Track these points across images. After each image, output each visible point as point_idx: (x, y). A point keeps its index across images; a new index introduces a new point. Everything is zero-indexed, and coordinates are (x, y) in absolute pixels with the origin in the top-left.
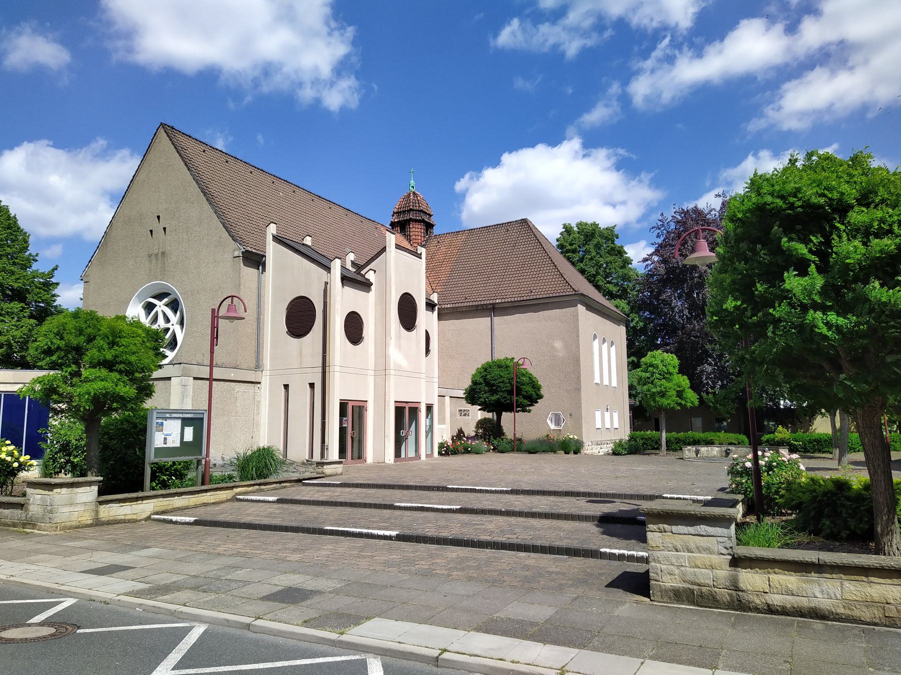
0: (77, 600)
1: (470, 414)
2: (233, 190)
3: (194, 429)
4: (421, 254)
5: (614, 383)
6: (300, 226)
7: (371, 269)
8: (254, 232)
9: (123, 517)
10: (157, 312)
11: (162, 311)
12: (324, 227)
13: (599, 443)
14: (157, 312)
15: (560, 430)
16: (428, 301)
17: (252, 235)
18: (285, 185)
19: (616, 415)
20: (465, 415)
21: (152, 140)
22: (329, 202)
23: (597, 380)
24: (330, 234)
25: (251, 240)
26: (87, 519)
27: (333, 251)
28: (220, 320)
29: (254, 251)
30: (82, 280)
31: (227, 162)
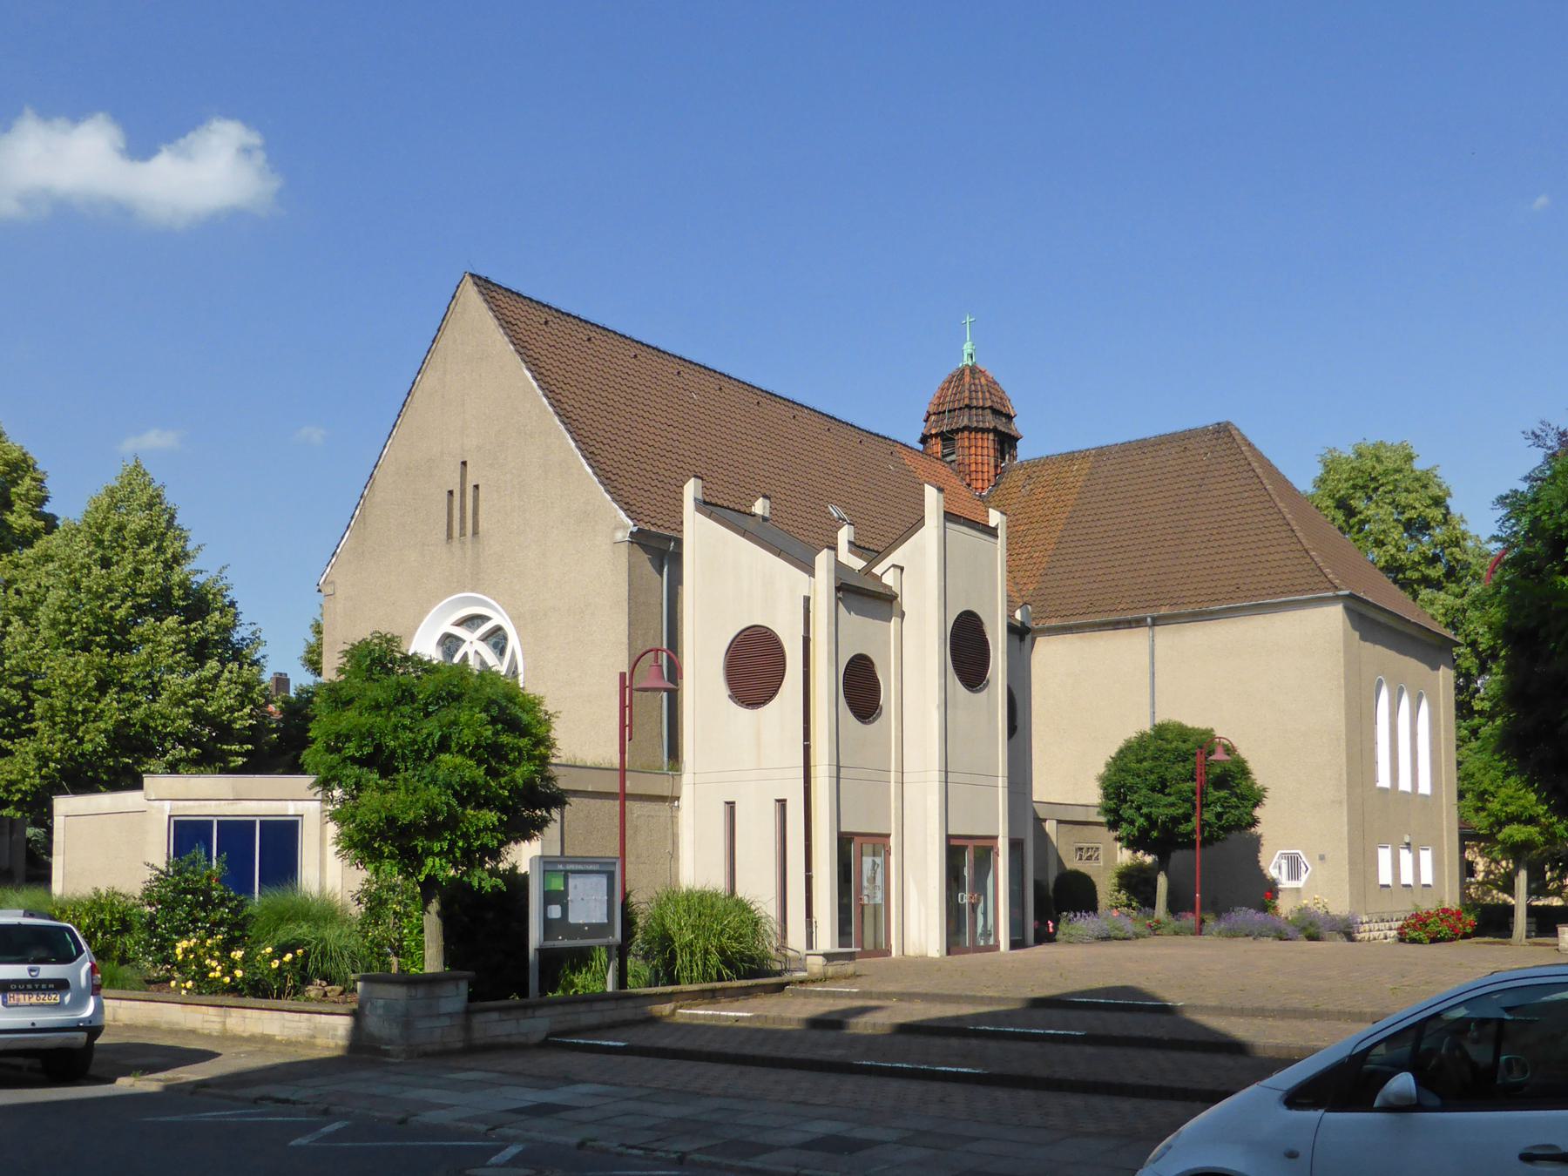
0: (489, 1163)
1: (1101, 857)
2: (606, 400)
3: (56, 794)
4: (996, 529)
5: (1425, 788)
6: (736, 464)
7: (894, 566)
8: (649, 487)
9: (505, 1039)
10: (466, 655)
11: (476, 652)
12: (785, 462)
13: (1386, 917)
14: (466, 655)
15: (1298, 890)
16: (1010, 620)
17: (646, 495)
18: (702, 376)
19: (1426, 857)
20: (1089, 858)
21: (448, 308)
22: (790, 405)
23: (1384, 781)
24: (797, 477)
25: (645, 507)
26: (456, 1040)
27: (804, 515)
28: (636, 694)
29: (653, 529)
30: (319, 591)
31: (589, 340)
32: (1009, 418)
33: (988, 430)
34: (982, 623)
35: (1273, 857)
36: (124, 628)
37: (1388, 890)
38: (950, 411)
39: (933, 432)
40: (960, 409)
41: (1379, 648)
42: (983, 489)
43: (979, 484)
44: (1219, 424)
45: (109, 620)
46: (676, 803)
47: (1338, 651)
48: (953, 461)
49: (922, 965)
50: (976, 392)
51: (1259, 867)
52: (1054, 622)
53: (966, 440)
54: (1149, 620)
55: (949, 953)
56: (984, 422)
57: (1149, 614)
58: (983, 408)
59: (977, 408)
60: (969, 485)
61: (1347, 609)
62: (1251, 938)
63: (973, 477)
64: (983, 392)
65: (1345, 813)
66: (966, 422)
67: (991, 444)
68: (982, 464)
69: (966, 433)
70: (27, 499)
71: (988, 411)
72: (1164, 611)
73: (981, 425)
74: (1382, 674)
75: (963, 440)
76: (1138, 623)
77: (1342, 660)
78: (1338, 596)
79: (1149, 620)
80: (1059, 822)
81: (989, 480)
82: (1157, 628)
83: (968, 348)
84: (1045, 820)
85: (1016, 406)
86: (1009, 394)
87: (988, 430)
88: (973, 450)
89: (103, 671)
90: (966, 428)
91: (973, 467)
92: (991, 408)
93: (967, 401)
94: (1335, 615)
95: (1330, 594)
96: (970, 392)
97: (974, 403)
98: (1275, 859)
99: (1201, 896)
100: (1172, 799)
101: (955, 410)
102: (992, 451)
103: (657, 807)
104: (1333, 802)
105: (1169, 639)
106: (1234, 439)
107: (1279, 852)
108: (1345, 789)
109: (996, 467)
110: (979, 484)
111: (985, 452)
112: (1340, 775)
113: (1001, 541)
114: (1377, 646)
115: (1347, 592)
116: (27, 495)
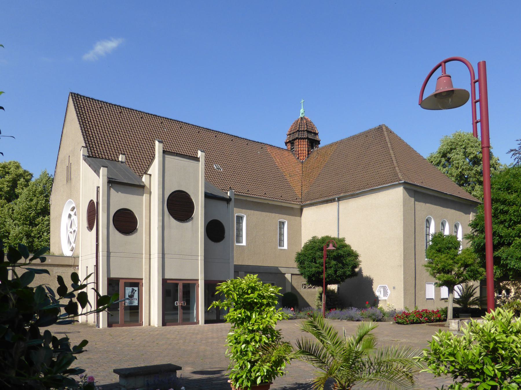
15: (385, 300)
32: (316, 134)
33: (305, 138)
34: (190, 196)
35: (377, 287)
36: (34, 218)
37: (433, 300)
38: (293, 133)
39: (288, 141)
40: (296, 132)
41: (428, 205)
42: (303, 159)
43: (302, 158)
44: (380, 126)
45: (28, 217)
46: (77, 268)
47: (401, 206)
48: (294, 150)
49: (154, 329)
50: (302, 125)
51: (373, 291)
52: (308, 202)
53: (297, 143)
54: (336, 199)
55: (164, 324)
56: (303, 136)
57: (336, 197)
58: (304, 131)
59: (301, 131)
60: (298, 158)
61: (405, 188)
62: (340, 320)
63: (300, 155)
64: (304, 125)
65: (403, 269)
66: (297, 136)
67: (306, 143)
68: (303, 150)
69: (297, 140)
70: (21, 185)
71: (306, 132)
72: (342, 195)
73: (302, 137)
74: (431, 215)
75: (296, 143)
76: (332, 201)
77: (402, 209)
78: (400, 183)
79: (336, 199)
80: (292, 274)
81: (305, 156)
82: (340, 202)
83: (302, 111)
84: (285, 274)
85: (318, 129)
86: (316, 126)
87: (305, 138)
88: (300, 146)
89: (27, 233)
90: (297, 138)
91: (300, 152)
92: (307, 130)
93: (298, 129)
94: (399, 191)
95: (397, 183)
96: (299, 126)
97: (301, 129)
98: (378, 289)
99: (100, 306)
100: (318, 265)
101: (294, 133)
102: (307, 146)
103: (66, 269)
104: (398, 266)
105: (345, 205)
106: (383, 130)
107: (379, 286)
108: (402, 261)
109: (308, 151)
110: (302, 158)
111: (304, 146)
112: (401, 255)
113: (201, 165)
114: (427, 204)
115: (403, 181)
116: (21, 184)
